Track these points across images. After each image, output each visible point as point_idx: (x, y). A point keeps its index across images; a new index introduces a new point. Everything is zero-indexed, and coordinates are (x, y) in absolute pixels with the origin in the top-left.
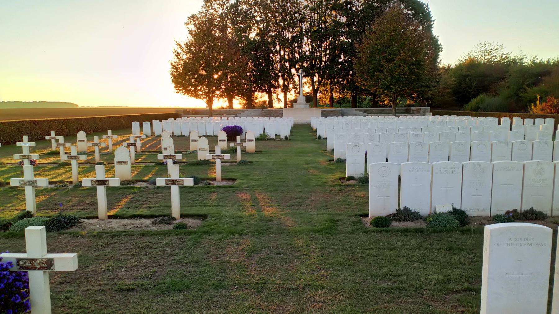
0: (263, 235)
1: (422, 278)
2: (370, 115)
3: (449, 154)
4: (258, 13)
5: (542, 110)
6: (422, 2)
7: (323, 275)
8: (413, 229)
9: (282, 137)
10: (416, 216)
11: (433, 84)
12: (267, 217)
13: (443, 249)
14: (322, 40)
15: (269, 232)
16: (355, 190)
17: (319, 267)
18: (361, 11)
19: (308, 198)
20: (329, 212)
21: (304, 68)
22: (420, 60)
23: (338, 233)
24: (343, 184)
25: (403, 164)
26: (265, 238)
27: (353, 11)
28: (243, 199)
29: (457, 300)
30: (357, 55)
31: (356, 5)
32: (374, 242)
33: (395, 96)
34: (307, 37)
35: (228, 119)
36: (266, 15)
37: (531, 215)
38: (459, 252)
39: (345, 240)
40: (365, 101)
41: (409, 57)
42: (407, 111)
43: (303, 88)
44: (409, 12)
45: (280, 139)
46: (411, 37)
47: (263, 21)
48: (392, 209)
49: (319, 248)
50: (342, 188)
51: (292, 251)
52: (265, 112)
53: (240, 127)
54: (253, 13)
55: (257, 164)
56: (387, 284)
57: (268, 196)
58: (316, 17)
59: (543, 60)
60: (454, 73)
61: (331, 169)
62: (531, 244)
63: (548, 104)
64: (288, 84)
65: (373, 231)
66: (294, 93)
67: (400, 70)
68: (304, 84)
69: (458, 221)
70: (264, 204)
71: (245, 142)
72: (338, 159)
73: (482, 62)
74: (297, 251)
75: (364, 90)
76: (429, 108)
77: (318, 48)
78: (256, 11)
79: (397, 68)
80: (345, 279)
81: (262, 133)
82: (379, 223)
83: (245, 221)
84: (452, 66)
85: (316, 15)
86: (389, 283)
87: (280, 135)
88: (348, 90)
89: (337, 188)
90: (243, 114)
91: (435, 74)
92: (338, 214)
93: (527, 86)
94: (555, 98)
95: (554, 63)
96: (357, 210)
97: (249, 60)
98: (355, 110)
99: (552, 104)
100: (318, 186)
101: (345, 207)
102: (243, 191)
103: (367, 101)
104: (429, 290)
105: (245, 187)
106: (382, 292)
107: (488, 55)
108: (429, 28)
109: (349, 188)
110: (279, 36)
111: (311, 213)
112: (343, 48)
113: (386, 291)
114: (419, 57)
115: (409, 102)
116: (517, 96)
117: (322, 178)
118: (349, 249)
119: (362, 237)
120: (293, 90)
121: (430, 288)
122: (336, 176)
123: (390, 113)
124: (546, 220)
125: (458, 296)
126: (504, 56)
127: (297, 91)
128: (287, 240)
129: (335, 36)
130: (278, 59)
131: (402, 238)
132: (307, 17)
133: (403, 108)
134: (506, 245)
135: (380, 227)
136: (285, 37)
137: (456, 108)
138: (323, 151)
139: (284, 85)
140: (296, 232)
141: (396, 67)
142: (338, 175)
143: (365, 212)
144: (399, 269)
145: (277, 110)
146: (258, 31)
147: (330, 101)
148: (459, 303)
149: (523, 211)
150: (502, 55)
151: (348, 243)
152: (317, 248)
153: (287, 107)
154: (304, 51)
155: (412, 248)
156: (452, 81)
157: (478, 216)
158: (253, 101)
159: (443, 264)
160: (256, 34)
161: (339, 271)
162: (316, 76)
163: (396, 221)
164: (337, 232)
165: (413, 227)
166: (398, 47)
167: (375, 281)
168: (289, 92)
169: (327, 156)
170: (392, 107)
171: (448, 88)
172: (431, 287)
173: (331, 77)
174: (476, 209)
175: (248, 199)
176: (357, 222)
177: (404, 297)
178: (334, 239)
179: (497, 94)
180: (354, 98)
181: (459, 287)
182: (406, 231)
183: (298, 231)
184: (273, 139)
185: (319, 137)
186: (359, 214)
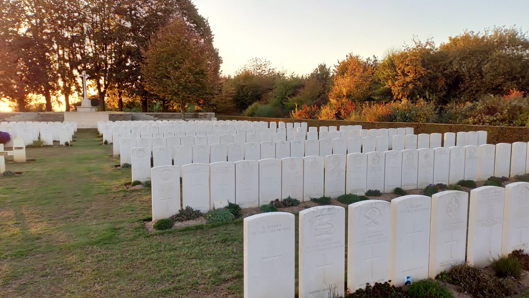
0: (27, 257)
1: (198, 274)
2: (160, 119)
3: (227, 155)
4: (28, 7)
5: (299, 115)
6: (203, 17)
7: (97, 291)
8: (194, 227)
9: (62, 143)
10: (197, 214)
11: (216, 92)
12: (34, 235)
13: (219, 242)
14: (106, 42)
15: (36, 252)
16: (140, 195)
17: (93, 283)
18: (145, 18)
19: (88, 208)
20: (111, 221)
21: (88, 70)
22: (203, 70)
23: (118, 243)
24: (129, 190)
25: (184, 166)
26: (28, 260)
27: (138, 17)
28: (4, 217)
29: (228, 289)
30: (143, 60)
31: (140, 12)
32: (156, 245)
33: (183, 102)
34: (89, 38)
35: (338, 129)
36: (39, 10)
37: (289, 202)
38: (232, 243)
39: (126, 248)
40: (155, 105)
41: (194, 66)
42: (196, 116)
43: (87, 91)
44: (192, 25)
45: (59, 145)
46: (194, 48)
47: (36, 16)
48: (175, 210)
49: (95, 262)
50: (127, 194)
51: (63, 270)
52: (42, 116)
53: (7, 133)
54: (22, 6)
55: (27, 175)
56: (164, 286)
57: (38, 210)
58: (97, 18)
59: (299, 76)
60: (234, 83)
61: (117, 175)
62: (280, 230)
63: (303, 111)
64: (70, 85)
65: (156, 235)
66: (77, 95)
67: (186, 78)
68: (89, 87)
69: (233, 215)
70: (31, 220)
71: (12, 150)
72: (125, 164)
73: (255, 75)
74: (68, 269)
75: (153, 95)
76: (214, 113)
77: (103, 50)
78: (27, 5)
79: (183, 76)
80: (121, 290)
81: (37, 139)
82: (162, 225)
83: (4, 243)
84: (232, 77)
85: (98, 17)
86: (167, 285)
87: (59, 141)
88: (137, 95)
89: (122, 194)
90: (13, 118)
91: (217, 83)
92: (120, 221)
93: (289, 96)
94: (308, 107)
95: (306, 78)
96: (141, 215)
97: (20, 58)
98: (146, 114)
99: (306, 111)
100: (100, 194)
101: (129, 213)
102: (6, 208)
103: (157, 106)
104: (204, 284)
105: (9, 203)
106: (159, 296)
107: (259, 69)
108: (209, 41)
109: (134, 194)
110: (56, 34)
111: (89, 224)
112: (129, 52)
113: (163, 294)
114: (202, 67)
115: (196, 107)
116: (282, 104)
117: (105, 185)
118: (129, 257)
119: (143, 242)
120: (76, 92)
121: (205, 282)
122: (121, 182)
123: (179, 118)
124: (299, 205)
125: (228, 285)
126: (271, 71)
127: (80, 94)
128: (57, 258)
129: (120, 39)
130: (56, 59)
131: (183, 237)
132: (88, 18)
133: (191, 113)
134: (261, 233)
135: (163, 229)
136: (64, 36)
137: (236, 114)
138: (109, 157)
139: (64, 87)
140: (70, 248)
141: (182, 74)
142: (123, 181)
143: (149, 216)
144: (178, 268)
145: (57, 114)
146: (30, 27)
147: (119, 105)
148: (229, 291)
149: (283, 200)
150: (269, 70)
151: (128, 250)
152: (92, 262)
153: (69, 111)
154: (86, 52)
155: (192, 245)
156: (232, 90)
157: (249, 208)
158: (26, 103)
159: (218, 256)
160: (27, 29)
161: (116, 283)
162: (101, 79)
163: (179, 221)
164: (117, 241)
165: (194, 225)
166: (182, 57)
167: (153, 286)
168: (71, 94)
169: (113, 161)
170: (180, 112)
171: (229, 97)
172: (206, 281)
173: (118, 80)
174: (248, 202)
175: (11, 216)
176: (140, 228)
177: (180, 296)
178: (113, 249)
179: (267, 103)
180: (144, 103)
181: (231, 276)
182: (187, 230)
183: (72, 246)
184: (51, 146)
185: (106, 143)
186: (143, 219)
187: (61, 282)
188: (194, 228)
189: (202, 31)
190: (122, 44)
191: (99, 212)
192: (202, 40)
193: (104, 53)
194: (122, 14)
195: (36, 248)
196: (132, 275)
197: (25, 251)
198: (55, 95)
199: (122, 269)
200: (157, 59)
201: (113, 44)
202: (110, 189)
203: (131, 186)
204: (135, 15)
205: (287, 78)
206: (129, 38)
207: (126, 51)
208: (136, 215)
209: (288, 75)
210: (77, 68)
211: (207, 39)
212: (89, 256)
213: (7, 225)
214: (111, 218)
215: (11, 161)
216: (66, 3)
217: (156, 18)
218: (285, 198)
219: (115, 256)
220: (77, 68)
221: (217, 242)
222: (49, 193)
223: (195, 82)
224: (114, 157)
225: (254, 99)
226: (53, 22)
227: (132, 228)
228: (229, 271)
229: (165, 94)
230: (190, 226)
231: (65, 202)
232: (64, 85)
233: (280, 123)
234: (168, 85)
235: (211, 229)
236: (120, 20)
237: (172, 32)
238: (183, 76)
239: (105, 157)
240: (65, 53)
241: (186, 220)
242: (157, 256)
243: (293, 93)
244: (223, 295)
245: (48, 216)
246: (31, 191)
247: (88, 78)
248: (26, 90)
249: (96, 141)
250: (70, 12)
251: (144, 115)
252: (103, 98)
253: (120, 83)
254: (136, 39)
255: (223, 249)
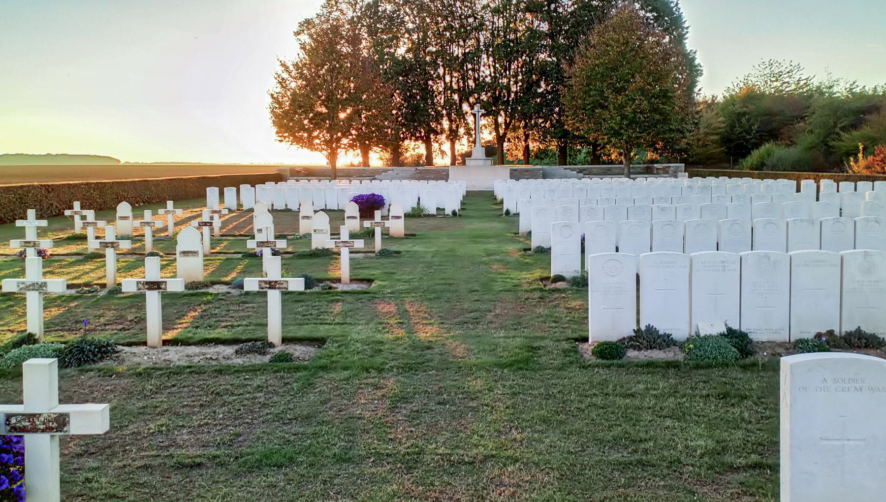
0: (417, 373)
1: (679, 445)
2: (587, 176)
4: (409, 16)
5: (868, 167)
8: (663, 363)
9: (448, 211)
10: (667, 342)
13: (712, 396)
14: (511, 58)
15: (427, 366)
18: (571, 13)
19: (490, 311)
22: (667, 90)
24: (547, 288)
27: (559, 13)
31: (563, 4)
32: (599, 384)
34: (487, 54)
37: (858, 339)
40: (580, 154)
41: (649, 84)
42: (648, 171)
44: (648, 15)
47: (418, 29)
48: (627, 329)
49: (508, 394)
50: (545, 294)
51: (465, 398)
52: (421, 172)
56: (621, 455)
58: (500, 23)
60: (723, 110)
62: (861, 389)
64: (457, 127)
66: (467, 141)
69: (736, 350)
70: (418, 320)
71: (388, 219)
72: (538, 247)
73: (767, 92)
74: (472, 399)
75: (578, 137)
76: (683, 165)
77: (505, 71)
79: (631, 103)
81: (415, 206)
83: (387, 349)
85: (501, 20)
86: (625, 454)
87: (444, 209)
89: (537, 295)
93: (842, 129)
96: (570, 331)
97: (396, 90)
98: (565, 169)
100: (505, 291)
103: (583, 155)
104: (693, 466)
105: (388, 293)
107: (777, 80)
108: (679, 40)
109: (556, 295)
111: (495, 335)
112: (544, 71)
115: (650, 155)
116: (826, 145)
117: (512, 279)
118: (558, 396)
119: (578, 375)
120: (466, 137)
122: (535, 275)
123: (620, 174)
129: (531, 52)
130: (441, 89)
131: (644, 378)
132: (487, 23)
133: (641, 166)
135: (608, 359)
139: (451, 129)
140: (471, 367)
141: (629, 100)
142: (538, 273)
143: (583, 334)
144: (641, 429)
147: (524, 155)
148: (744, 489)
149: (843, 334)
150: (799, 81)
151: (556, 385)
152: (504, 394)
155: (661, 394)
156: (720, 122)
160: (406, 49)
161: (543, 433)
164: (538, 366)
166: (631, 70)
167: (602, 450)
168: (459, 140)
169: (520, 242)
170: (623, 164)
171: (713, 134)
173: (525, 116)
175: (392, 312)
177: (650, 477)
179: (793, 143)
180: (563, 150)
181: (743, 462)
182: (650, 365)
183: (474, 365)
184: (433, 216)
185: (508, 213)
187: (464, 417)
188: (664, 365)
189: (667, 23)
190: (533, 59)
191: (507, 318)
192: (667, 39)
193: (506, 74)
194: (536, 12)
195: (428, 361)
196: (566, 425)
197: (414, 363)
198: (437, 142)
199: (548, 413)
200: (588, 77)
201: (520, 59)
202: (519, 285)
203: (550, 282)
204: (555, 10)
205: (838, 95)
206: (545, 46)
207: (539, 69)
208: (562, 330)
209: (840, 90)
210: (468, 101)
211: (675, 37)
212: (499, 384)
213: (389, 324)
214: (525, 330)
215: (387, 235)
216: (458, 4)
217: (589, 12)
218: (849, 331)
219: (537, 390)
220: (468, 101)
221: (708, 395)
222: (437, 284)
223: (650, 111)
224: (520, 235)
225: (764, 137)
226: (439, 35)
227: (558, 350)
228: (738, 452)
229: (599, 135)
230: (654, 360)
231: (459, 299)
232: (449, 127)
233: (823, 183)
234: (604, 120)
235: (694, 371)
236: (532, 21)
237: (615, 31)
238: (631, 103)
239: (508, 235)
240: (454, 79)
241: (647, 349)
242: (603, 402)
243: (854, 122)
244: (732, 494)
245: (439, 316)
246: (413, 278)
247: (483, 115)
248: (402, 136)
249: (492, 210)
250: (463, 17)
251: (560, 169)
252: (502, 144)
253: (527, 121)
254: (556, 48)
255: (722, 411)
